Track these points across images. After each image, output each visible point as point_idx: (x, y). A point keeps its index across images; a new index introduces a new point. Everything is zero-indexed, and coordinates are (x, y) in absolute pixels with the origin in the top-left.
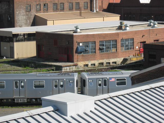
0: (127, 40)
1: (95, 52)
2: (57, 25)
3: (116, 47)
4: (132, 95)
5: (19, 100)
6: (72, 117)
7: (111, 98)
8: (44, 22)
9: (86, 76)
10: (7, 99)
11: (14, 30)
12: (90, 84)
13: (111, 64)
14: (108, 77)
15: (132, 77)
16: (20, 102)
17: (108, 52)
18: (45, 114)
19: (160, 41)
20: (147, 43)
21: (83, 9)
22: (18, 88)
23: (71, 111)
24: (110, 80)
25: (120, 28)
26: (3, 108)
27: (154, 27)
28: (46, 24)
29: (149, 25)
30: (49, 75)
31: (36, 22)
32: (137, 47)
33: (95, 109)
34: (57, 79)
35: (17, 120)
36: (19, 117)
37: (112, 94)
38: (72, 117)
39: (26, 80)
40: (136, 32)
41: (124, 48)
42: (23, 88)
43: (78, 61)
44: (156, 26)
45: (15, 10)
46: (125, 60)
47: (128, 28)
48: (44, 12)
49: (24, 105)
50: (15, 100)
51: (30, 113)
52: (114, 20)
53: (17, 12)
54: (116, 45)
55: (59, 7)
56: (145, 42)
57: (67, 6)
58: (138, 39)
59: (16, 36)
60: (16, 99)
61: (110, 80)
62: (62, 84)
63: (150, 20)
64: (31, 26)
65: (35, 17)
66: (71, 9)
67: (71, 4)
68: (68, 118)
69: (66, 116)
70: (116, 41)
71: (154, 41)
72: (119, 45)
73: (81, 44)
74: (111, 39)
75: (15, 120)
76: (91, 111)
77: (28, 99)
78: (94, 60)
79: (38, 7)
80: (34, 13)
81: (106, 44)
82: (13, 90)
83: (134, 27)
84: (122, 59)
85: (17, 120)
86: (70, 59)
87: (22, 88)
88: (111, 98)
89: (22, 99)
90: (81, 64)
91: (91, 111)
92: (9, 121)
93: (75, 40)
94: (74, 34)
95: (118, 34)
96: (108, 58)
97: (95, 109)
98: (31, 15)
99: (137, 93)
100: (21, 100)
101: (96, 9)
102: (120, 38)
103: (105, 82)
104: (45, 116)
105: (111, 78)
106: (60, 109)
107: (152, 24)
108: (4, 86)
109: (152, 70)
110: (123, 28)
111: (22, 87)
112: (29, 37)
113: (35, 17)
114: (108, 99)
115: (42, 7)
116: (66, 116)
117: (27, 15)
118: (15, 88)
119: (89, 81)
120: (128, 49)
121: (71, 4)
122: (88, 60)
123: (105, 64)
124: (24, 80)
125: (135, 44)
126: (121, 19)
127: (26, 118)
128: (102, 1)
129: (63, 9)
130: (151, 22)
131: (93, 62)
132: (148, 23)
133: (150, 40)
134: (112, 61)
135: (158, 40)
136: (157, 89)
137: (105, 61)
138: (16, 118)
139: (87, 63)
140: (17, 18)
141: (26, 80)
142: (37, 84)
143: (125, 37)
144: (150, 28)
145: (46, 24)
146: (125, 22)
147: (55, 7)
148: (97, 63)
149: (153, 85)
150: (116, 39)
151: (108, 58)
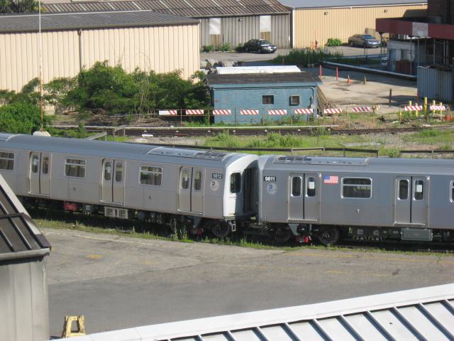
5: (111, 211)
10: (80, 205)
12: (268, 187)
16: (114, 216)
22: (406, 197)
24: (326, 181)
30: (335, 160)
34: (407, 176)
35: (423, 306)
36: (431, 298)
39: (432, 177)
42: (422, 198)
49: (347, 245)
50: (103, 210)
60: (106, 208)
61: (326, 181)
62: (313, 188)
75: (417, 306)
77: (435, 231)
82: (394, 206)
85: (423, 306)
87: (419, 201)
89: (118, 210)
92: (398, 307)
100: (116, 211)
104: (413, 316)
108: (369, 191)
111: (311, 193)
118: (399, 199)
119: (268, 179)
124: (316, 174)
127: (427, 308)
138: (420, 302)
141: (432, 177)
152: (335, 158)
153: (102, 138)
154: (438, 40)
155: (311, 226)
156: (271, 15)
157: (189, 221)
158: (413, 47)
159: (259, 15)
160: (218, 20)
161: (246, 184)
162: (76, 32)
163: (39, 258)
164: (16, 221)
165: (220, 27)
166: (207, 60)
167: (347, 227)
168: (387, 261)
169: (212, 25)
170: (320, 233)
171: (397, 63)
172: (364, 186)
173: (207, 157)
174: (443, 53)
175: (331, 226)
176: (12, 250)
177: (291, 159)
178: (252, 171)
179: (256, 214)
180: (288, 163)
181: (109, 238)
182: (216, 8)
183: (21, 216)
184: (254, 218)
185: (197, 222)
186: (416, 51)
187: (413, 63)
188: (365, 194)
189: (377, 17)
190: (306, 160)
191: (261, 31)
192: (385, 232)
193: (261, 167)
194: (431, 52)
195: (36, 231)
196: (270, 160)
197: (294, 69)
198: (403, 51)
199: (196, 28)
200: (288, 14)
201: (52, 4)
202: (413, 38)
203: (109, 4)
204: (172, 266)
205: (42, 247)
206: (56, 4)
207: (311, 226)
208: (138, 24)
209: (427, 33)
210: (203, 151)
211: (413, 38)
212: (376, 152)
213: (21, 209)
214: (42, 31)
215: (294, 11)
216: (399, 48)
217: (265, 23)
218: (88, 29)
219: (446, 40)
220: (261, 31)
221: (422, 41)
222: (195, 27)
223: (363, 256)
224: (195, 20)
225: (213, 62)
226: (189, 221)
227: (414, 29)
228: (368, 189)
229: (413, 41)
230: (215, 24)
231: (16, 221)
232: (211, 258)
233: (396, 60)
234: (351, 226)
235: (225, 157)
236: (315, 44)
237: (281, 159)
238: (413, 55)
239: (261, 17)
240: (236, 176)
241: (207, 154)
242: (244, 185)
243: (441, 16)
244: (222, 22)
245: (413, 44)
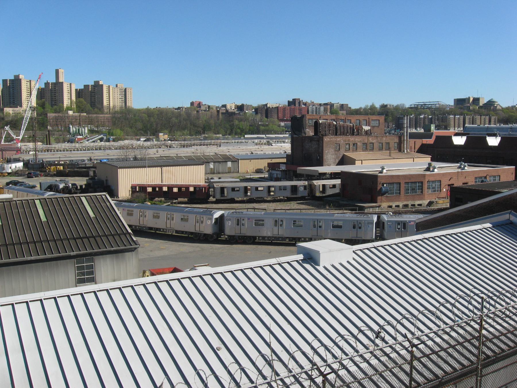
0: (433, 182)
1: (400, 193)
2: (365, 165)
3: (422, 189)
4: (400, 245)
6: (325, 267)
7: (375, 248)
8: (352, 162)
9: (385, 217)
11: (321, 169)
13: (416, 206)
14: (407, 220)
15: (417, 223)
17: (112, 203)
18: (240, 271)
19: (469, 184)
20: (455, 185)
21: (392, 149)
23: (325, 261)
25: (428, 169)
26: (86, 276)
27: (463, 169)
28: (354, 163)
29: (459, 167)
31: (343, 161)
32: (444, 190)
33: (354, 259)
37: (409, 239)
38: (325, 267)
40: (444, 174)
41: (430, 191)
43: (381, 202)
44: (466, 168)
45: (324, 149)
46: (430, 204)
47: (436, 170)
48: (353, 151)
51: (279, 261)
52: (426, 160)
53: (326, 151)
54: (422, 187)
55: (369, 148)
56: (453, 185)
57: (376, 146)
58: (445, 182)
59: (325, 174)
63: (291, 141)
64: (337, 165)
65: (344, 156)
66: (381, 149)
67: (380, 144)
68: (321, 268)
69: (319, 265)
70: (422, 183)
71: (463, 184)
72: (425, 186)
73: (385, 185)
74: (416, 181)
76: (348, 262)
78: (399, 201)
79: (347, 146)
80: (342, 152)
81: (415, 184)
83: (443, 168)
84: (429, 201)
86: (374, 200)
88: (375, 248)
90: (385, 205)
91: (348, 262)
93: (379, 179)
94: (380, 174)
95: (424, 176)
96: (414, 200)
97: (354, 259)
98: (340, 154)
99: (407, 244)
101: (407, 150)
102: (427, 180)
103: (404, 225)
105: (410, 222)
106: (311, 258)
107: (462, 166)
109: (437, 217)
110: (431, 170)
112: (334, 176)
113: (344, 156)
114: (372, 249)
115: (351, 146)
116: (319, 265)
117: (336, 154)
120: (435, 191)
121: (380, 144)
122: (392, 201)
123: (410, 206)
125: (442, 186)
126: (432, 160)
128: (71, 84)
129: (372, 149)
130: (461, 165)
131: (397, 203)
132: (459, 165)
133: (458, 183)
134: (417, 203)
135: (466, 183)
136: (431, 239)
137: (410, 203)
139: (391, 204)
140: (325, 157)
142: (336, 223)
143: (432, 179)
144: (460, 170)
145: (354, 163)
146: (434, 164)
147: (365, 146)
148: (426, 202)
149: (427, 235)
150: (422, 180)
151: (413, 200)
153: (169, 205)
160: (213, 163)
162: (159, 169)
163: (136, 248)
164: (128, 236)
172: (262, 222)
175: (250, 236)
176: (125, 246)
178: (222, 217)
179: (224, 232)
182: (212, 159)
183: (129, 234)
185: (202, 235)
188: (263, 225)
189: (133, 183)
193: (225, 215)
195: (134, 239)
196: (229, 213)
198: (277, 174)
199: (204, 166)
205: (136, 245)
213: (130, 231)
214: (149, 167)
217: (229, 164)
218: (167, 166)
221: (284, 171)
225: (210, 178)
231: (128, 236)
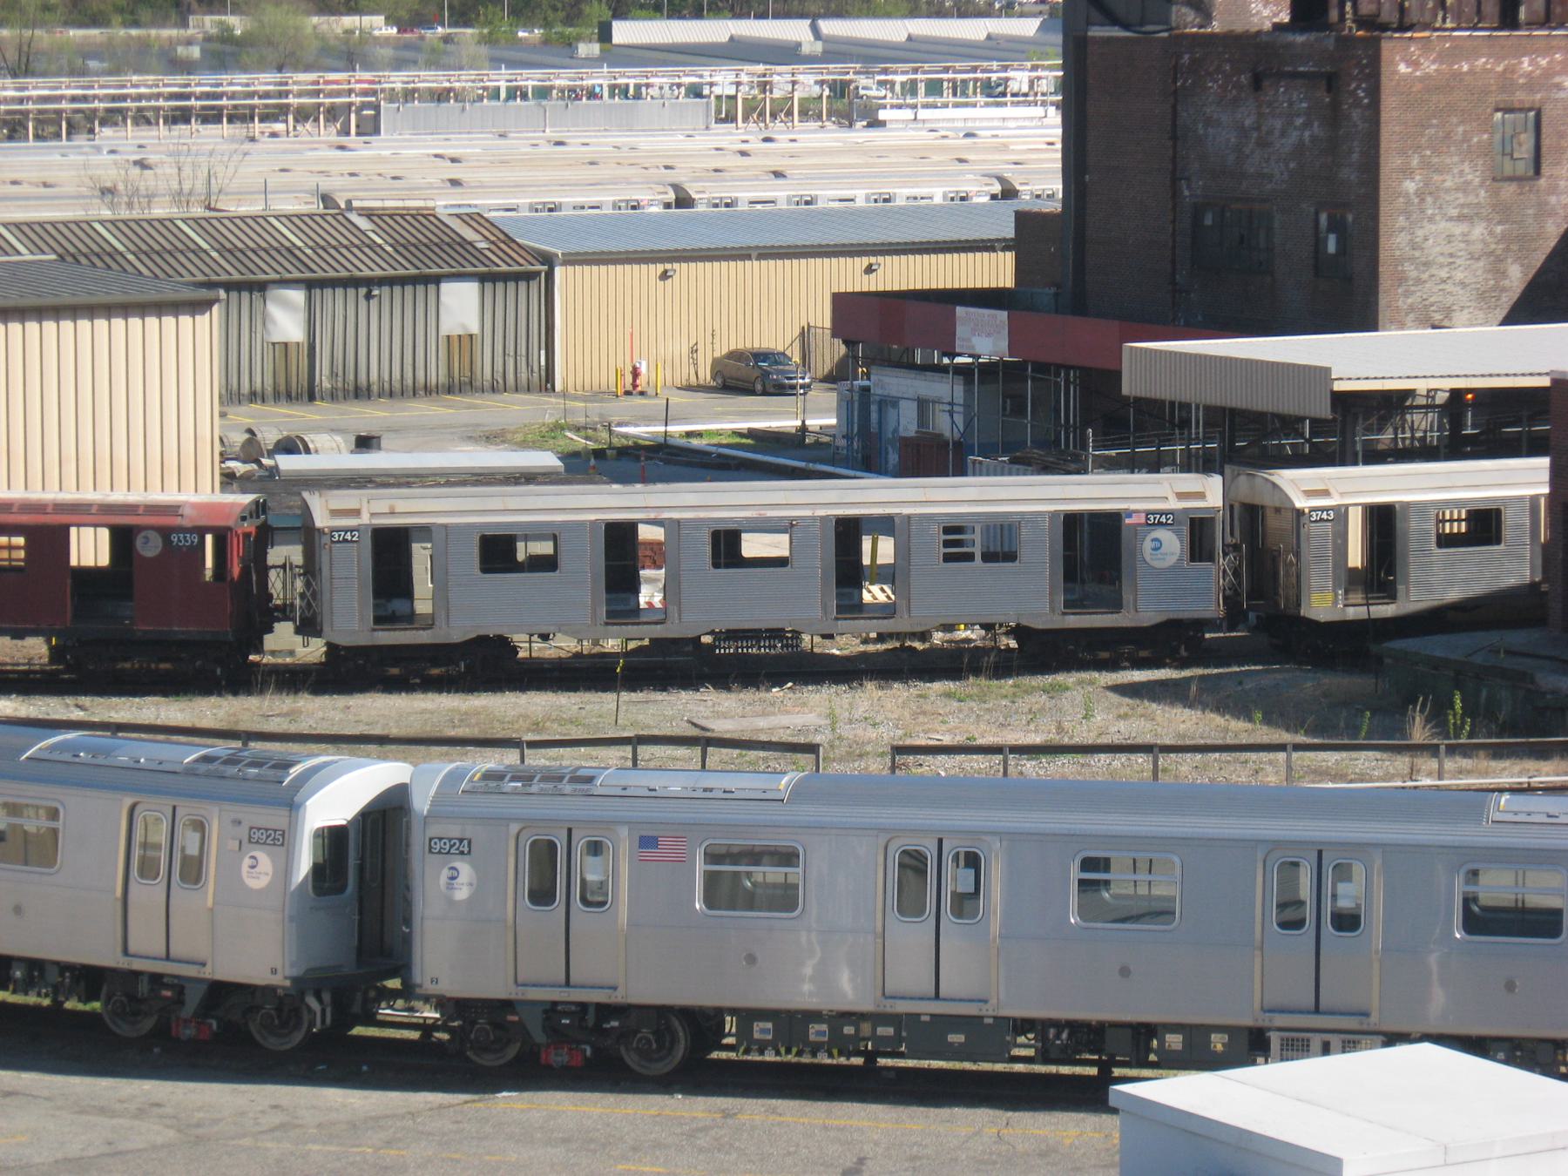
22: (920, 911)
152: (673, 775)
154: (1042, 368)
155: (592, 1010)
156: (483, 278)
157: (168, 993)
158: (959, 390)
159: (437, 280)
160: (297, 296)
161: (369, 860)
165: (301, 316)
166: (250, 431)
167: (719, 1013)
168: (825, 1128)
169: (274, 310)
170: (624, 1035)
171: (906, 442)
172: (772, 874)
173: (232, 770)
174: (1058, 411)
177: (526, 777)
178: (386, 817)
180: (515, 792)
181: (1520, 774)
184: (394, 983)
186: (967, 406)
187: (957, 444)
190: (576, 779)
191: (444, 332)
192: (849, 1030)
193: (421, 803)
194: (1019, 410)
196: (453, 778)
197: (749, 441)
198: (923, 404)
200: (538, 273)
201: (170, 220)
202: (959, 360)
203: (272, 220)
204: (74, 1149)
206: (101, 222)
207: (592, 1010)
208: (93, 300)
209: (1004, 345)
210: (221, 748)
211: (959, 360)
212: (812, 748)
215: (558, 271)
216: (911, 393)
217: (461, 305)
219: (1068, 368)
220: (444, 332)
221: (989, 371)
222: (203, 320)
223: (741, 1111)
224: (204, 294)
226: (168, 993)
227: (961, 331)
228: (791, 880)
229: (962, 370)
230: (286, 305)
232: (216, 1121)
233: (903, 433)
234: (733, 1011)
235: (295, 771)
236: (629, 378)
237: (488, 776)
238: (959, 419)
239: (447, 288)
240: (334, 838)
241: (232, 761)
242: (361, 869)
243: (1058, 286)
244: (309, 300)
245: (960, 379)
